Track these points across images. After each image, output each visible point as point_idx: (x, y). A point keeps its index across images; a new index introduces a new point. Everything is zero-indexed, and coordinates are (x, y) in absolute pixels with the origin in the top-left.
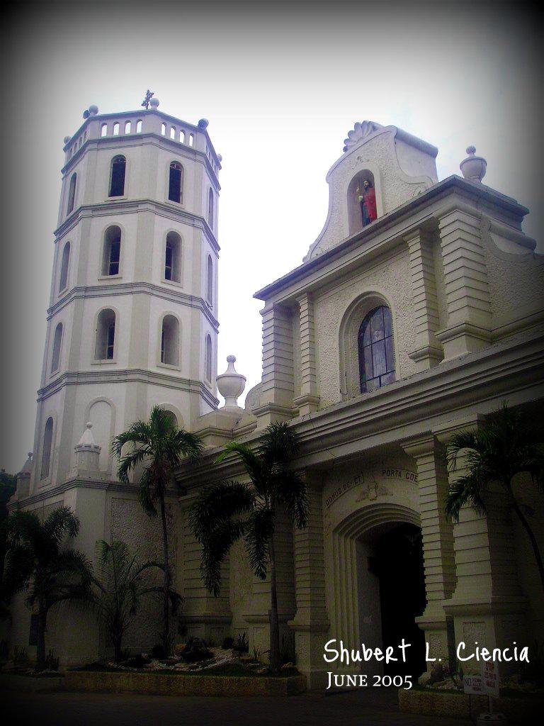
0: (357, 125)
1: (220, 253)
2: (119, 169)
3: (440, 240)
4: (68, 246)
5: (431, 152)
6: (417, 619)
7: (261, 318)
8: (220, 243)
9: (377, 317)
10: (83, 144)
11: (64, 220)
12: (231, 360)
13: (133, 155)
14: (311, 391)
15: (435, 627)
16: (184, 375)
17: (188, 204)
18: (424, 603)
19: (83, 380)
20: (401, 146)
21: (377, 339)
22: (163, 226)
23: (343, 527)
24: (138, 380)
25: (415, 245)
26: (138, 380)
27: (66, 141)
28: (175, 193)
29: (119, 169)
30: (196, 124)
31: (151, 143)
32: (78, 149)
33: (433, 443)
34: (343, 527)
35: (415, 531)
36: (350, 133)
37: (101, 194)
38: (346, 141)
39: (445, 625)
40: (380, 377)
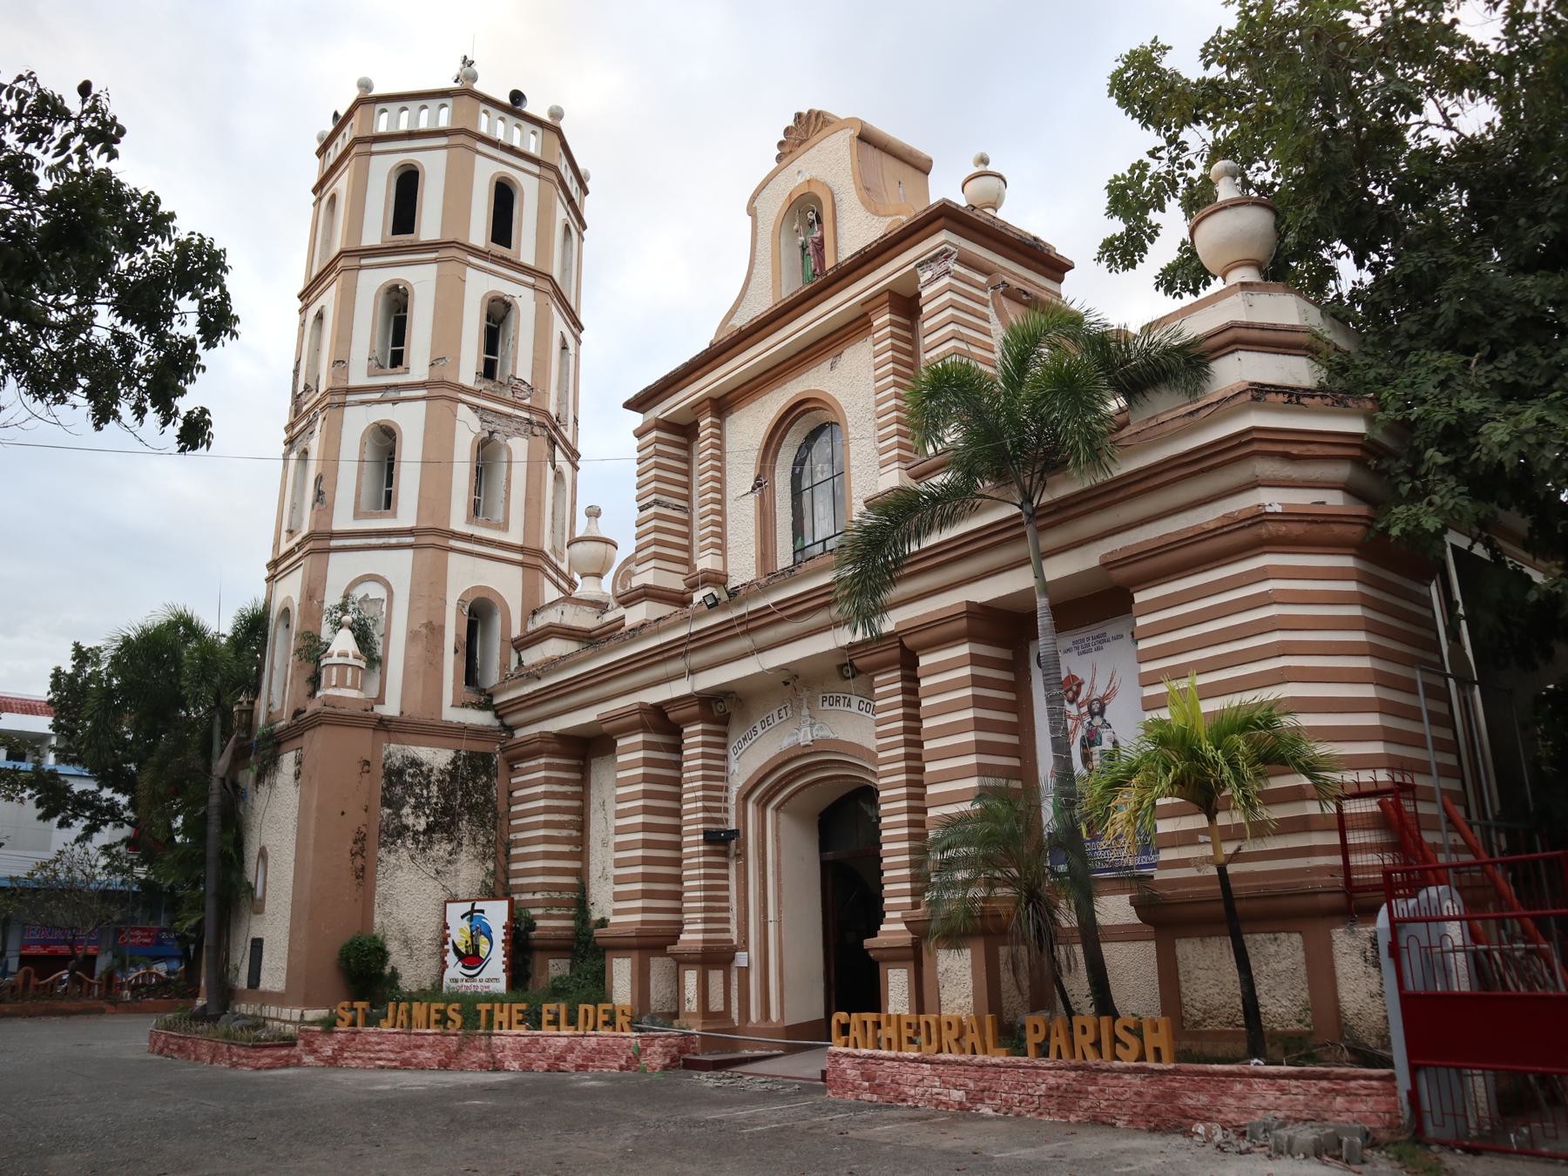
0: (799, 116)
1: (583, 336)
2: (407, 184)
3: (920, 310)
4: (320, 317)
5: (922, 167)
6: (868, 943)
7: (636, 442)
8: (583, 320)
9: (824, 438)
10: (347, 142)
11: (315, 273)
12: (593, 513)
13: (433, 165)
14: (525, 539)
15: (896, 956)
16: (515, 536)
17: (525, 247)
18: (878, 917)
19: (334, 543)
20: (873, 154)
21: (819, 478)
22: (480, 285)
23: (1545, 883)
24: (433, 546)
25: (883, 319)
26: (433, 546)
27: (320, 139)
28: (502, 229)
29: (407, 184)
30: (506, 100)
31: (461, 145)
32: (339, 151)
33: (898, 650)
34: (1545, 883)
35: (868, 794)
36: (787, 131)
37: (375, 230)
38: (781, 144)
39: (910, 952)
40: (824, 541)
